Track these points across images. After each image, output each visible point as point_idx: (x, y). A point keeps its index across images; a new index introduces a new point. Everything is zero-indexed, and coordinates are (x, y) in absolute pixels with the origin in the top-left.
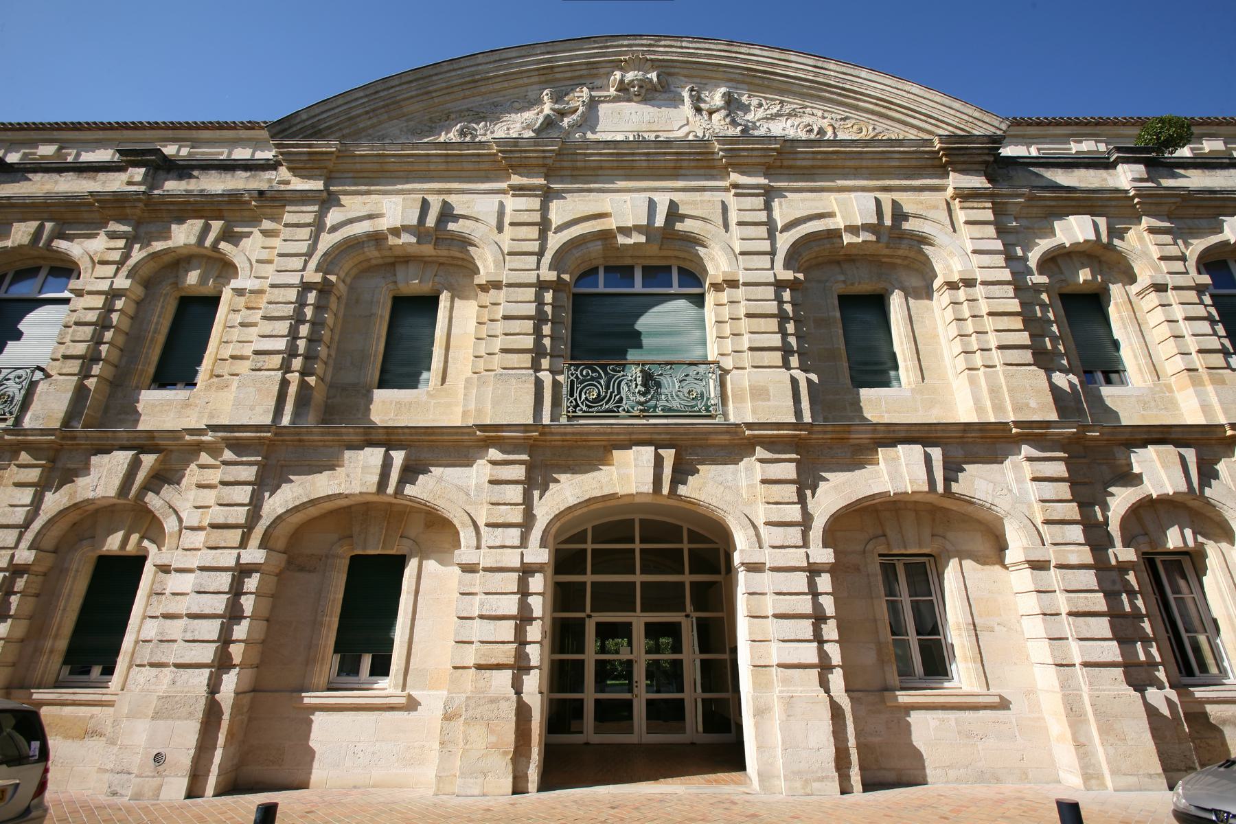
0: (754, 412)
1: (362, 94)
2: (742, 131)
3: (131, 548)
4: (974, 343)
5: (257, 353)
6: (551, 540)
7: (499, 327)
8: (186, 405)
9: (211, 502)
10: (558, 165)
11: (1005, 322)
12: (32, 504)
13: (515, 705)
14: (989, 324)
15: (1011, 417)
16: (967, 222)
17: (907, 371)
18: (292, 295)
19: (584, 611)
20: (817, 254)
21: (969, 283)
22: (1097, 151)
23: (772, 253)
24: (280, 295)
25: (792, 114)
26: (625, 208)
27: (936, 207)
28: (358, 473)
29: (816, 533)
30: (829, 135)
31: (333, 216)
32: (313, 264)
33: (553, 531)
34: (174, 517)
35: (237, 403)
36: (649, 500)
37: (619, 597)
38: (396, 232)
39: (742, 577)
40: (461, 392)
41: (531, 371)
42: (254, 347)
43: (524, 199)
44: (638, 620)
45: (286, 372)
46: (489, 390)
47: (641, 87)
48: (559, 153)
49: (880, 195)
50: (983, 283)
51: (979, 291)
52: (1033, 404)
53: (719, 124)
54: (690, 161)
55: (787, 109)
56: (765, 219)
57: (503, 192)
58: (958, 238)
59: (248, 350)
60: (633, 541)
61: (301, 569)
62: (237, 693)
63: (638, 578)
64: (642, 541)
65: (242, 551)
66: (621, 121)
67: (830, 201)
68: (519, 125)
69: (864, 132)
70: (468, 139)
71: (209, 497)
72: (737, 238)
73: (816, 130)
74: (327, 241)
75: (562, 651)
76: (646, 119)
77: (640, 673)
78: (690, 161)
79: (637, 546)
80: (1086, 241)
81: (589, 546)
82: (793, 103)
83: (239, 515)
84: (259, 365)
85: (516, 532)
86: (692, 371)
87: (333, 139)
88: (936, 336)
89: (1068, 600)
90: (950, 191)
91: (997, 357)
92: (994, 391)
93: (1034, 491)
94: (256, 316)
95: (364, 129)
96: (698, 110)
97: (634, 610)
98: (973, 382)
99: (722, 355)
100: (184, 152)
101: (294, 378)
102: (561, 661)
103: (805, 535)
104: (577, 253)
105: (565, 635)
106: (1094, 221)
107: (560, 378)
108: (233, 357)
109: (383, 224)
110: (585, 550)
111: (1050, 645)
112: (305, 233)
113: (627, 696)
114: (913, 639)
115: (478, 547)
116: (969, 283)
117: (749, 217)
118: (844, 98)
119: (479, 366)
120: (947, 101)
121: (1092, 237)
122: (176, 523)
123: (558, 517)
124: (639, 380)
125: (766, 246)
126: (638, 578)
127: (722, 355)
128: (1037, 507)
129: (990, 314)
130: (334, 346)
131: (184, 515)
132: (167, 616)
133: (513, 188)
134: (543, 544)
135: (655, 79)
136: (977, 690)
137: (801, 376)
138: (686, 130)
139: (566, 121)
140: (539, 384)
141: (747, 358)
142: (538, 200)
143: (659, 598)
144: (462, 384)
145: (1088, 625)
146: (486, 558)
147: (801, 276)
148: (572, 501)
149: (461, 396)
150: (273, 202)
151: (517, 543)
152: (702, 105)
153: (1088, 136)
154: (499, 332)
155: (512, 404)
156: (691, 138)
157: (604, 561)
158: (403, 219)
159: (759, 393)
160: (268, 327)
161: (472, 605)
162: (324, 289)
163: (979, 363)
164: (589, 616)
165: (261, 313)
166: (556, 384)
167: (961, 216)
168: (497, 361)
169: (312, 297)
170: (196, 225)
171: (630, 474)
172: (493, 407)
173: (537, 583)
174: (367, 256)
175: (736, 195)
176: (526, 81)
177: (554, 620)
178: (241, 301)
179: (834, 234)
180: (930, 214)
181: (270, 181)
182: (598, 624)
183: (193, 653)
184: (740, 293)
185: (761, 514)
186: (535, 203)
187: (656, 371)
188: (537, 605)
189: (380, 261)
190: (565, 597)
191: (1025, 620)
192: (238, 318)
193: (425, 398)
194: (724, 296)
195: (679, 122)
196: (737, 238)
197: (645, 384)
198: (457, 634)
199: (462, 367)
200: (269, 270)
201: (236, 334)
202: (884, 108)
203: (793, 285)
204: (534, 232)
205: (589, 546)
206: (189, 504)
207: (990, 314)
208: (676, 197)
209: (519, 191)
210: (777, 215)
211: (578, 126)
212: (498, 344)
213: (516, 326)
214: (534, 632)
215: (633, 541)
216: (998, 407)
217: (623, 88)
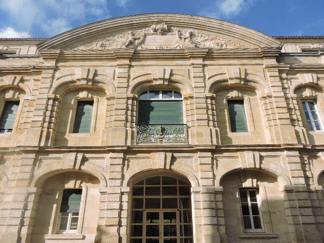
0: (198, 141)
1: (68, 34)
2: (195, 46)
3: (77, 187)
4: (271, 117)
5: (33, 121)
6: (131, 184)
7: (114, 113)
8: (9, 138)
9: (18, 171)
10: (134, 57)
11: (281, 110)
12: (30, 179)
13: (118, 238)
14: (276, 111)
15: (282, 143)
16: (271, 76)
17: (250, 126)
18: (45, 101)
19: (143, 208)
20: (219, 88)
21: (270, 97)
22: (239, 97)
23: (205, 87)
24: (40, 102)
25: (212, 39)
26: (156, 72)
27: (259, 71)
28: (66, 162)
29: (125, 182)
30: (224, 47)
31: (58, 75)
32: (51, 91)
33: (131, 181)
34: (5, 177)
35: (27, 138)
36: (163, 170)
37: (154, 204)
38: (79, 80)
39: (193, 196)
40: (101, 134)
41: (124, 128)
42: (32, 119)
43: (122, 69)
44: (161, 211)
45: (43, 128)
46: (110, 134)
47: (161, 30)
48: (134, 53)
49: (241, 67)
50: (274, 97)
51: (273, 100)
52: (290, 138)
53: (188, 44)
54: (179, 55)
55: (211, 37)
56: (203, 76)
57: (115, 66)
58: (266, 81)
59: (30, 120)
60: (160, 184)
61: (48, 194)
62: (27, 235)
63: (161, 197)
64: (146, 184)
65: (29, 188)
66: (154, 42)
67: (225, 69)
68: (120, 43)
69: (236, 45)
70: (103, 48)
71: (18, 170)
72: (194, 83)
73: (220, 45)
74: (56, 83)
75: (136, 222)
76: (163, 41)
77: (161, 230)
78: (179, 55)
79: (161, 186)
80: (310, 83)
81: (145, 186)
82: (213, 35)
83: (28, 176)
84: (34, 126)
85: (119, 181)
86: (178, 127)
87: (58, 50)
88: (260, 115)
89: (299, 203)
90: (264, 66)
91: (278, 122)
92: (277, 133)
93: (289, 167)
94: (33, 109)
95: (69, 45)
96: (181, 38)
97: (160, 208)
98: (270, 131)
99: (188, 121)
100: (5, 48)
101: (45, 130)
102: (135, 226)
103: (122, 183)
104: (140, 87)
105: (136, 217)
106: (312, 76)
107: (134, 129)
108: (24, 123)
109: (75, 78)
110: (143, 187)
111: (293, 218)
112: (49, 81)
113: (141, 224)
114: (251, 216)
115: (107, 186)
116: (270, 97)
117: (197, 75)
118: (229, 33)
119: (106, 122)
120: (264, 36)
121: (312, 81)
122: (6, 178)
123: (133, 176)
124: (160, 131)
125: (203, 85)
126: (161, 197)
127: (188, 121)
128: (290, 172)
129: (277, 107)
130: (58, 119)
131: (9, 176)
132: (3, 209)
133: (118, 65)
134: (128, 185)
135: (166, 28)
136: (269, 233)
137: (213, 129)
138: (177, 45)
139: (137, 41)
140: (127, 131)
141: (196, 123)
142: (127, 69)
143: (168, 204)
144: (101, 131)
145: (305, 211)
146: (109, 190)
147: (214, 95)
148: (137, 171)
149: (101, 136)
150: (37, 70)
151: (119, 185)
152: (182, 36)
153: (317, 43)
154: (114, 114)
155: (119, 140)
156: (178, 48)
157: (150, 191)
158: (82, 76)
159: (200, 135)
160: (37, 113)
161: (105, 206)
162: (55, 99)
163: (273, 124)
164: (144, 210)
165: (34, 108)
166: (133, 132)
167: (268, 74)
168: (113, 124)
169: (51, 102)
170: (13, 77)
171: (156, 162)
172: (112, 140)
173: (125, 198)
174: (69, 89)
175: (193, 67)
176: (123, 28)
177: (132, 212)
178: (27, 104)
179: (226, 81)
180: (258, 73)
181: (37, 62)
182: (147, 213)
183: (13, 222)
184: (194, 101)
185: (199, 176)
186: (126, 70)
187: (166, 127)
188: (125, 206)
189: (74, 90)
190: (136, 203)
191: (286, 210)
192: (26, 109)
193: (89, 136)
194: (189, 102)
195: (173, 41)
196: (194, 83)
197: (162, 132)
198: (100, 215)
199: (101, 126)
200: (37, 92)
201: (25, 115)
202: (243, 38)
203: (212, 98)
204: (125, 80)
205: (145, 186)
206: (10, 172)
207: (277, 107)
208: (173, 68)
209: (120, 66)
210: (206, 74)
211: (141, 44)
212: (113, 118)
213: (119, 112)
214: (124, 214)
215: (160, 184)
216: (278, 139)
217: (155, 31)
